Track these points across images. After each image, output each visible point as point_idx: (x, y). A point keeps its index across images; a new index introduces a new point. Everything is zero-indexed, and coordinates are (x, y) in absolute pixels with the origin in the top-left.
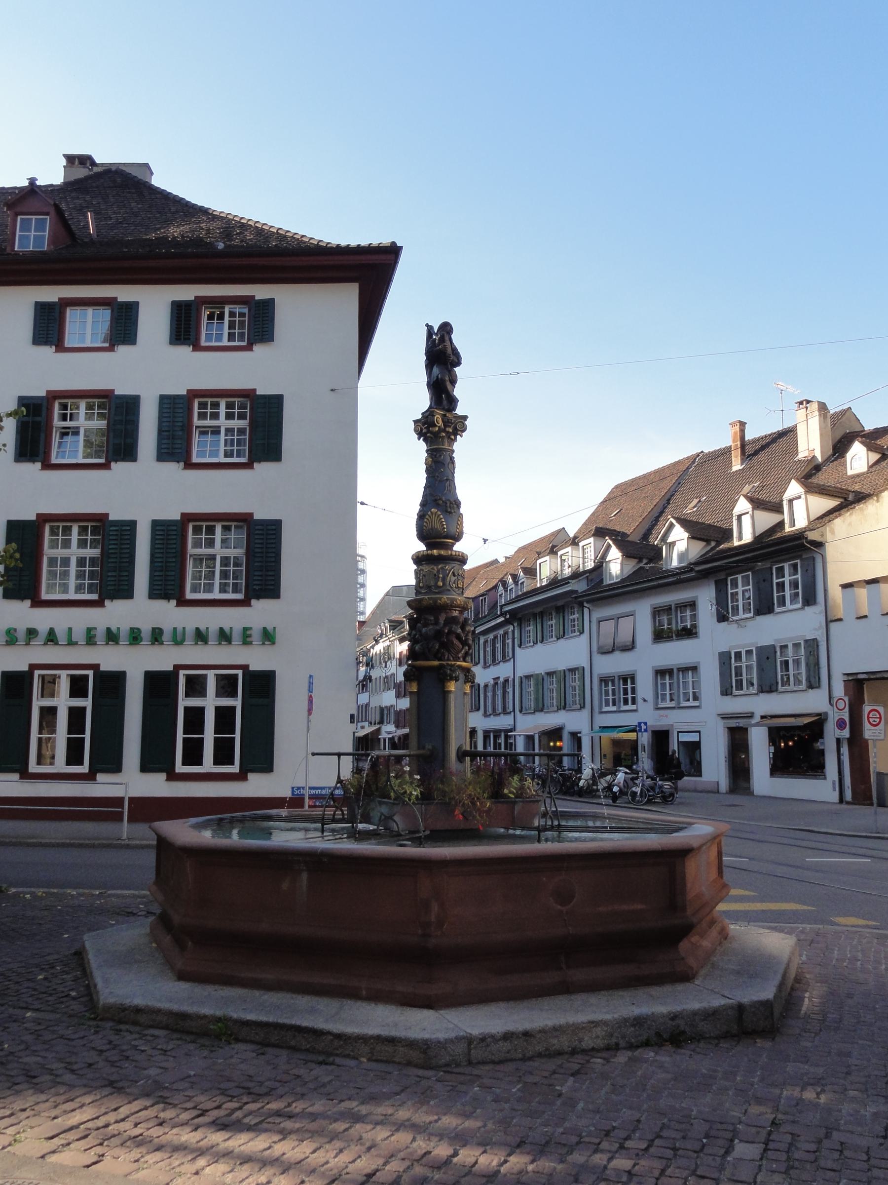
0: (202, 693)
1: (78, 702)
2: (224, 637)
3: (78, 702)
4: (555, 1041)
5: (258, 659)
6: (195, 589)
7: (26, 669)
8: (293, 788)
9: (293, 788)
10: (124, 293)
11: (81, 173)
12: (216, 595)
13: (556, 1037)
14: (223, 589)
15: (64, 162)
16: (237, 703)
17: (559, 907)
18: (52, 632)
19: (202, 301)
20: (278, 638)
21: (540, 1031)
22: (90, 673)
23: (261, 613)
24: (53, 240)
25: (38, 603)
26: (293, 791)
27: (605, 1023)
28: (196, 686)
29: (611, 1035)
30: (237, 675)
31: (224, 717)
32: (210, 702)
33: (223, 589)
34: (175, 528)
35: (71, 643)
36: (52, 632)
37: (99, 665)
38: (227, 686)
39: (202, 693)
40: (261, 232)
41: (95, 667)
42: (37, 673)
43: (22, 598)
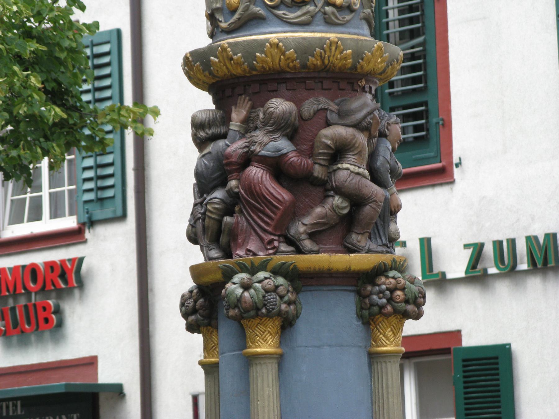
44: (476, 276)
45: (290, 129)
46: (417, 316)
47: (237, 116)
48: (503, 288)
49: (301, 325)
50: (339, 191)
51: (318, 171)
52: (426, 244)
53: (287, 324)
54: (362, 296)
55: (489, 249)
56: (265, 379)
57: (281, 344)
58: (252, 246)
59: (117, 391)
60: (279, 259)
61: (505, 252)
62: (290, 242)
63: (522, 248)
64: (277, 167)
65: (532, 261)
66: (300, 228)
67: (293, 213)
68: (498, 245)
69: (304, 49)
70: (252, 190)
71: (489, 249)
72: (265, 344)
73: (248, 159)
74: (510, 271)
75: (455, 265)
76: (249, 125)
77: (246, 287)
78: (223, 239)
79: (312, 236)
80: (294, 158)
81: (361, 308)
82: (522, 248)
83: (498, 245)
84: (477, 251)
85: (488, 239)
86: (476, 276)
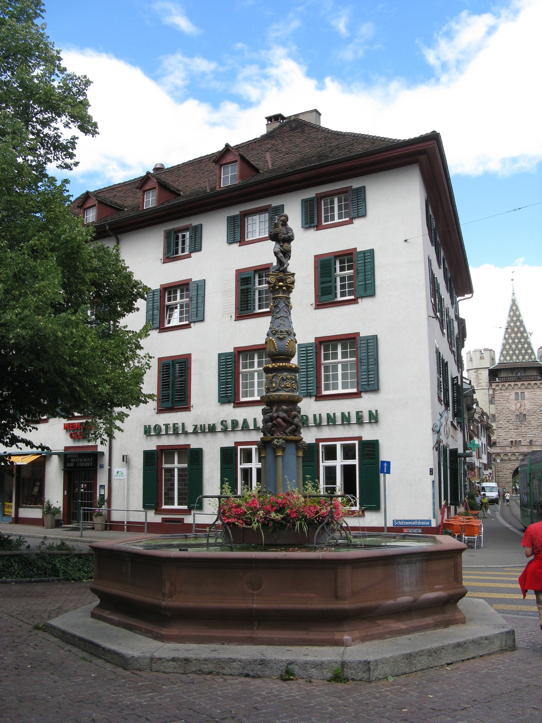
0: (334, 458)
1: (247, 465)
2: (346, 420)
3: (247, 465)
4: (205, 666)
5: (368, 434)
6: (327, 388)
7: (233, 445)
8: (394, 520)
9: (394, 520)
10: (275, 202)
11: (276, 125)
12: (340, 391)
13: (206, 664)
14: (344, 386)
15: (266, 121)
16: (355, 462)
17: (251, 591)
18: (245, 421)
19: (320, 197)
20: (380, 418)
21: (195, 659)
22: (356, 442)
23: (366, 403)
24: (242, 176)
25: (238, 405)
26: (394, 523)
27: (240, 661)
28: (331, 453)
29: (244, 668)
30: (355, 444)
31: (348, 471)
32: (339, 463)
33: (344, 386)
34: (311, 348)
35: (186, 433)
36: (245, 421)
37: (361, 437)
38: (348, 452)
39: (334, 458)
40: (374, 140)
41: (359, 438)
42: (321, 444)
43: (229, 402)
44: (195, 432)
45: (285, 411)
46: (24, 430)
47: (274, 409)
48: (201, 436)
49: (286, 450)
50: (294, 424)
51: (291, 420)
52: (183, 424)
53: (284, 449)
54: (297, 445)
55: (199, 426)
56: (280, 461)
57: (283, 453)
58: (278, 434)
59: (102, 454)
60: (284, 437)
61: (203, 428)
62: (285, 434)
63: (207, 426)
64: (284, 419)
65: (209, 429)
66: (287, 431)
67: (286, 428)
68: (201, 425)
69: (290, 396)
70: (279, 423)
71: (199, 426)
72: (280, 454)
73: (278, 417)
74: (203, 432)
75: (190, 430)
76: (277, 411)
77: (278, 442)
78: (271, 432)
79: (289, 433)
80: (287, 418)
81: (296, 447)
82: (207, 426)
83: (201, 425)
84: (196, 426)
85: (199, 424)
86: (195, 432)
